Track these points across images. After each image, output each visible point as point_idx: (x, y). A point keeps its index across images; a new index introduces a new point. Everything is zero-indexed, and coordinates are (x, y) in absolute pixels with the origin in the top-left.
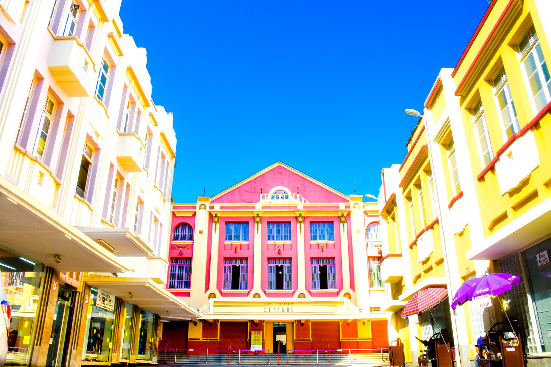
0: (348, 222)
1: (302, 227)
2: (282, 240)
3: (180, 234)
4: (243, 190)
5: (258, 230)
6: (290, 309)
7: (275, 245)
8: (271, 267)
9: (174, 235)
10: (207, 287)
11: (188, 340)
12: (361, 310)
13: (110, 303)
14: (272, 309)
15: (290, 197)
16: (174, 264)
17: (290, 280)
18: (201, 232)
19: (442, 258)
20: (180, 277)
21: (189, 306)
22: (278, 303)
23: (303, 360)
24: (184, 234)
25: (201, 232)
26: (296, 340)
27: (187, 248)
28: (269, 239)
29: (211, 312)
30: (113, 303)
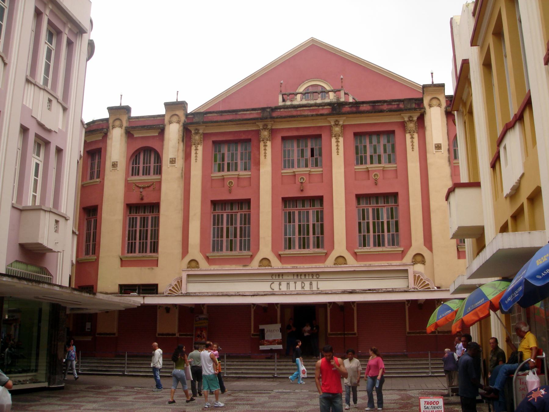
1: (339, 144)
3: (141, 165)
6: (314, 283)
7: (295, 175)
9: (133, 167)
10: (185, 250)
11: (157, 336)
16: (134, 215)
17: (396, 232)
18: (114, 165)
20: (144, 236)
22: (294, 275)
23: (257, 369)
25: (114, 165)
26: (331, 334)
27: (151, 188)
28: (285, 167)
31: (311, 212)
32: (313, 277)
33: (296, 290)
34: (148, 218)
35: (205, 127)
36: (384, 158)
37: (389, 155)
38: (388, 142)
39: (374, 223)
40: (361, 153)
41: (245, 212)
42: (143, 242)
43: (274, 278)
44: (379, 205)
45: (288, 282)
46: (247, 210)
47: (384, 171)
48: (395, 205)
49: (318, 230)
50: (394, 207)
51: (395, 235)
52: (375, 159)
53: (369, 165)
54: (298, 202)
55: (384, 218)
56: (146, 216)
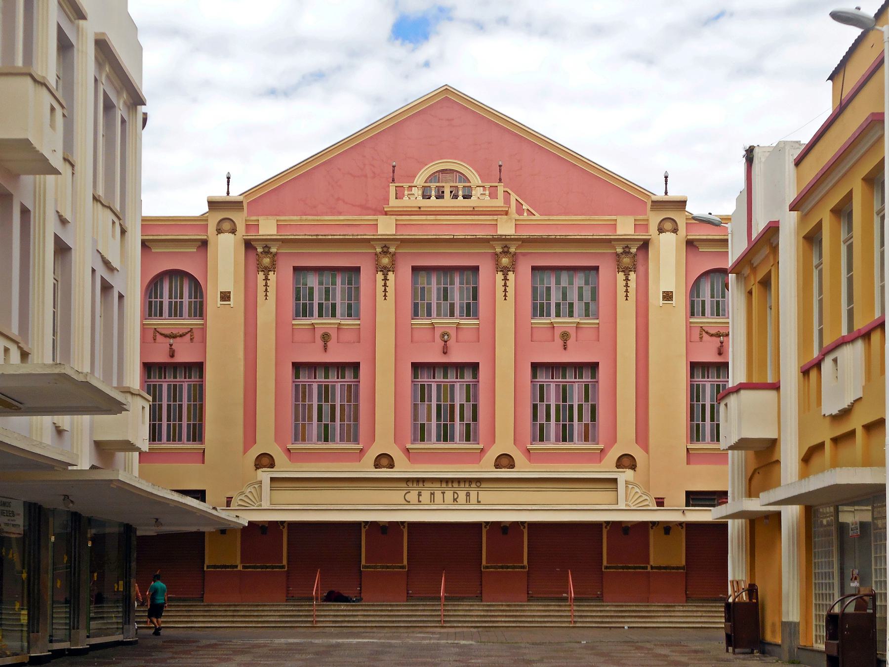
0: (641, 268)
2: (452, 314)
4: (339, 169)
5: (385, 291)
8: (423, 386)
10: (250, 437)
11: (205, 569)
12: (660, 502)
13: (12, 520)
14: (426, 495)
15: (477, 193)
19: (882, 418)
20: (175, 413)
21: (214, 508)
23: (506, 616)
24: (179, 300)
26: (487, 567)
29: (265, 504)
30: (20, 521)
31: (457, 386)
32: (470, 485)
33: (445, 503)
34: (334, 387)
35: (281, 242)
36: (578, 307)
37: (587, 304)
38: (587, 283)
39: (558, 407)
40: (304, 299)
41: (712, 381)
42: (174, 425)
43: (411, 485)
44: (178, 379)
45: (432, 492)
46: (198, 380)
47: (339, 328)
48: (592, 380)
49: (468, 414)
50: (590, 383)
51: (157, 425)
52: (565, 309)
53: (554, 319)
54: (710, 369)
55: (459, 399)
56: (178, 383)
